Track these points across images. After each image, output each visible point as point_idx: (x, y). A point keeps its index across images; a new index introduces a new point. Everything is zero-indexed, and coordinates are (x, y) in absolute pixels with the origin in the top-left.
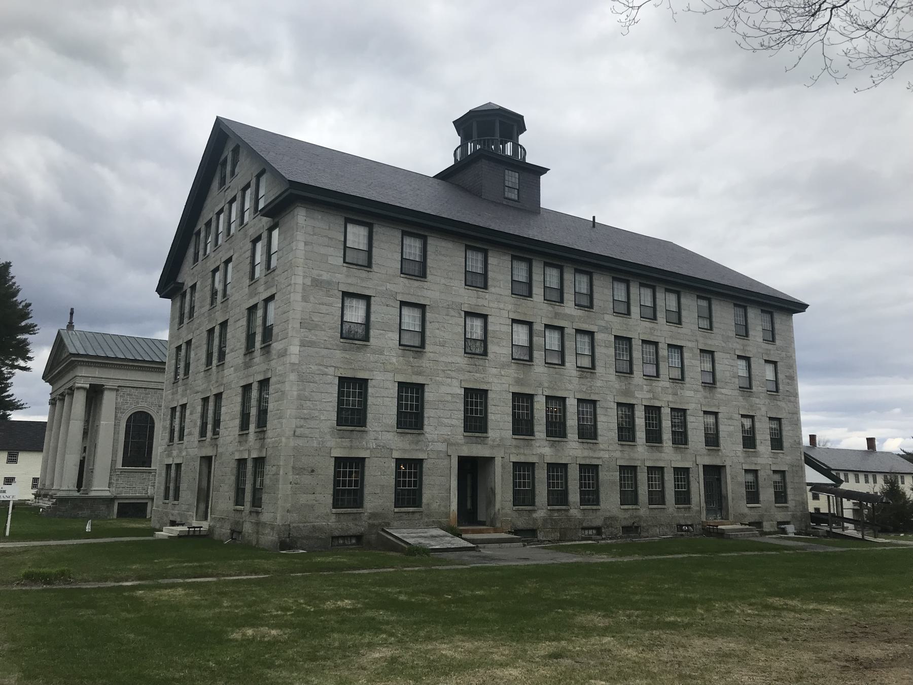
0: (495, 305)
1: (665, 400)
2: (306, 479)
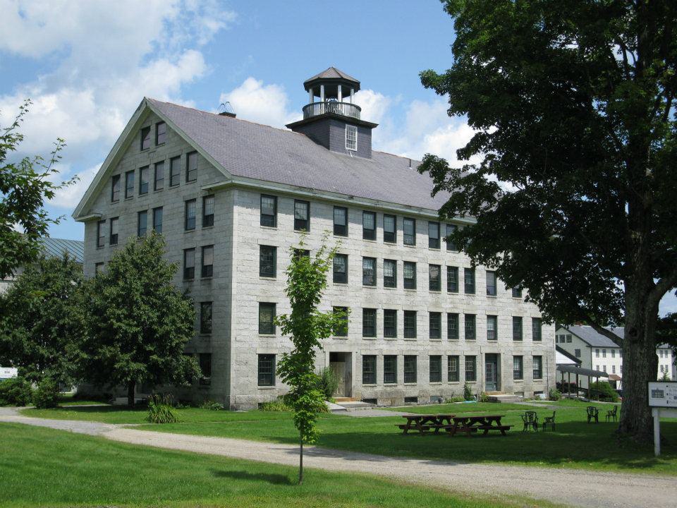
0: (353, 247)
1: (462, 311)
2: (244, 368)
